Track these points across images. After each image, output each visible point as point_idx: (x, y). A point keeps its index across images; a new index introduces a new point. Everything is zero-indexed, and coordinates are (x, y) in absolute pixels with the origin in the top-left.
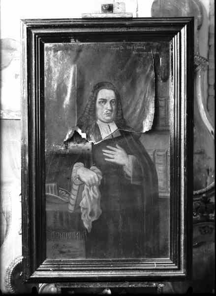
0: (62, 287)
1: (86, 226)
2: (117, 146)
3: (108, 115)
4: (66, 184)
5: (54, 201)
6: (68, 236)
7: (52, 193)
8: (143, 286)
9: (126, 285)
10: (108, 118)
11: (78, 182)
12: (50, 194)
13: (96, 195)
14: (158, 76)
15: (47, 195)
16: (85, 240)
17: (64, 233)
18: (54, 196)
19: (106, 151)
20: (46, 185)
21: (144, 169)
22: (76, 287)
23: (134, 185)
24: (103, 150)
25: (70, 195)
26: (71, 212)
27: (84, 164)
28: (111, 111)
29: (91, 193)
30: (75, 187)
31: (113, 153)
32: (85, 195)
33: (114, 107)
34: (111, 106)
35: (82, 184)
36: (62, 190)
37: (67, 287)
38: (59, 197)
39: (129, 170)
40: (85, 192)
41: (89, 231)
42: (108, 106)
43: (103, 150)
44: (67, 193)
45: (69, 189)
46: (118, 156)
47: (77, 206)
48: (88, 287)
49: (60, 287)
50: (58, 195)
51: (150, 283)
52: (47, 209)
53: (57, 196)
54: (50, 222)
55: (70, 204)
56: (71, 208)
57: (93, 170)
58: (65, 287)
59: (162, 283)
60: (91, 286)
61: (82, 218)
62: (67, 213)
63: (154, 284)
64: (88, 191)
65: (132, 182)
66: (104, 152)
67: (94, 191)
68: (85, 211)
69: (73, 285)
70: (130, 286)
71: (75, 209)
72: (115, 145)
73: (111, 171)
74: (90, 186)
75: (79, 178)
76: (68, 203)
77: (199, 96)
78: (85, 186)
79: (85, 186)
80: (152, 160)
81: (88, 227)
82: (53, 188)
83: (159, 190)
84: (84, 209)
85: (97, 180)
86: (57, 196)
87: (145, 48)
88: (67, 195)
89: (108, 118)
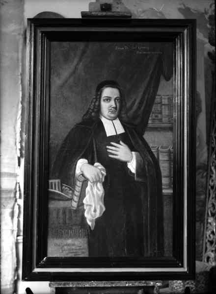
0: (57, 286)
1: (90, 223)
2: (121, 142)
3: (112, 112)
4: (68, 177)
5: (56, 197)
6: (71, 234)
7: (55, 189)
8: (140, 285)
9: (122, 284)
10: (113, 115)
11: (82, 179)
12: (53, 190)
13: (99, 190)
14: (143, 146)
15: (51, 192)
16: (88, 238)
17: (67, 230)
18: (57, 193)
19: (110, 147)
20: (50, 181)
21: (151, 157)
22: (71, 286)
23: (138, 182)
24: (107, 147)
25: (73, 191)
26: (75, 209)
27: (88, 161)
28: (116, 108)
29: (95, 190)
30: (79, 184)
31: (117, 149)
32: (88, 192)
33: (118, 105)
34: (116, 104)
35: (86, 181)
36: (66, 187)
37: (62, 286)
38: (63, 194)
39: (132, 167)
40: (88, 189)
41: (92, 229)
42: (112, 103)
43: (107, 147)
44: (71, 190)
45: (72, 186)
46: (120, 151)
47: (81, 204)
48: (83, 286)
49: (55, 286)
50: (62, 192)
51: (148, 282)
52: (49, 206)
53: (60, 193)
54: (53, 217)
55: (74, 200)
56: (75, 204)
57: (96, 167)
58: (60, 286)
59: (159, 282)
60: (145, 244)
61: (86, 215)
62: (70, 211)
63: (152, 283)
64: (92, 189)
65: (135, 178)
66: (109, 149)
67: (98, 188)
68: (88, 207)
69: (68, 284)
70: (127, 285)
71: (78, 206)
72: (119, 141)
73: (115, 168)
74: (94, 182)
75: (83, 175)
76: (71, 199)
77: (99, 284)
78: (89, 182)
79: (89, 183)
80: (156, 156)
81: (92, 225)
82: (57, 184)
83: (163, 187)
84: (87, 205)
85: (101, 176)
86: (60, 193)
87: (148, 48)
88: (71, 192)
89: (113, 115)
